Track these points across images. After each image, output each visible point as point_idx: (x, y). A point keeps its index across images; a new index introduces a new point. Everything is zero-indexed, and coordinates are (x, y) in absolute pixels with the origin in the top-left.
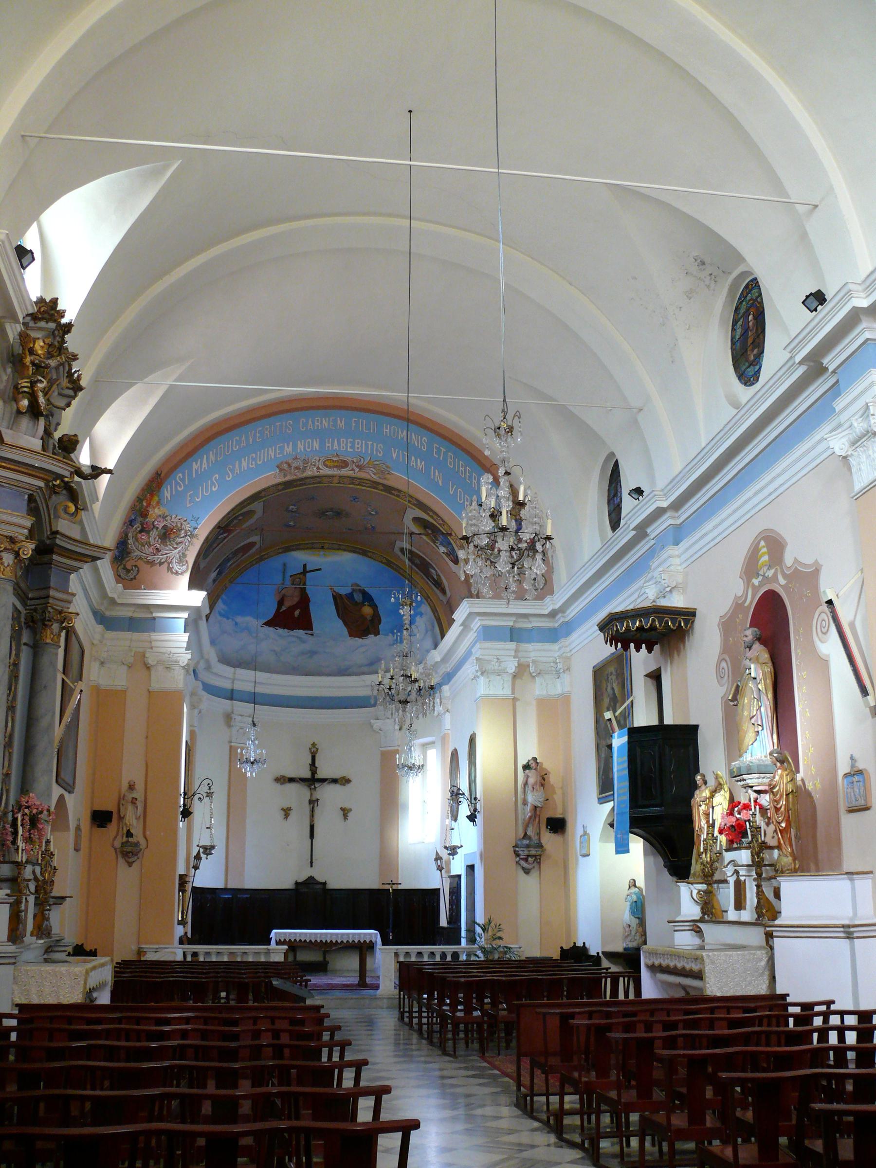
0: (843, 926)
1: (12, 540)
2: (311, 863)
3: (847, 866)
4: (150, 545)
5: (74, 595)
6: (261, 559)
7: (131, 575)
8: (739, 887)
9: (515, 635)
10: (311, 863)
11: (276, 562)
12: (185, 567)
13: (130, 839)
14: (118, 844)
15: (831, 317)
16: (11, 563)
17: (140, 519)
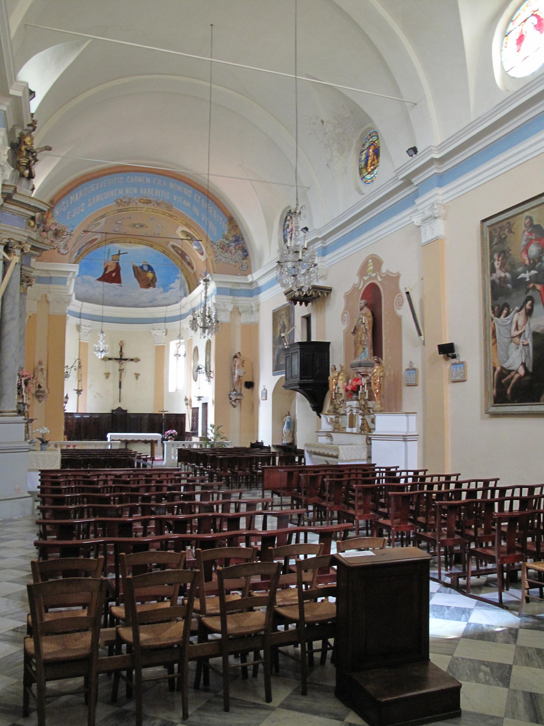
0: (403, 436)
1: (20, 243)
2: (120, 400)
3: (405, 410)
4: (48, 239)
8: (352, 417)
9: (232, 292)
10: (120, 400)
12: (67, 251)
13: (40, 389)
15: (419, 161)
17: (42, 225)
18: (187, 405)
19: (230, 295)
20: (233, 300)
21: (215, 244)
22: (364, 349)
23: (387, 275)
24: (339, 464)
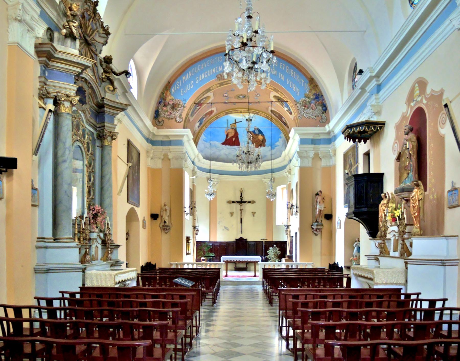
0: (441, 260)
5: (116, 125)
6: (217, 118)
7: (161, 124)
9: (314, 142)
11: (224, 118)
14: (161, 226)
16: (69, 106)
17: (163, 101)
18: (287, 234)
19: (312, 144)
20: (313, 148)
21: (298, 103)
22: (408, 174)
23: (432, 95)
24: (375, 287)
